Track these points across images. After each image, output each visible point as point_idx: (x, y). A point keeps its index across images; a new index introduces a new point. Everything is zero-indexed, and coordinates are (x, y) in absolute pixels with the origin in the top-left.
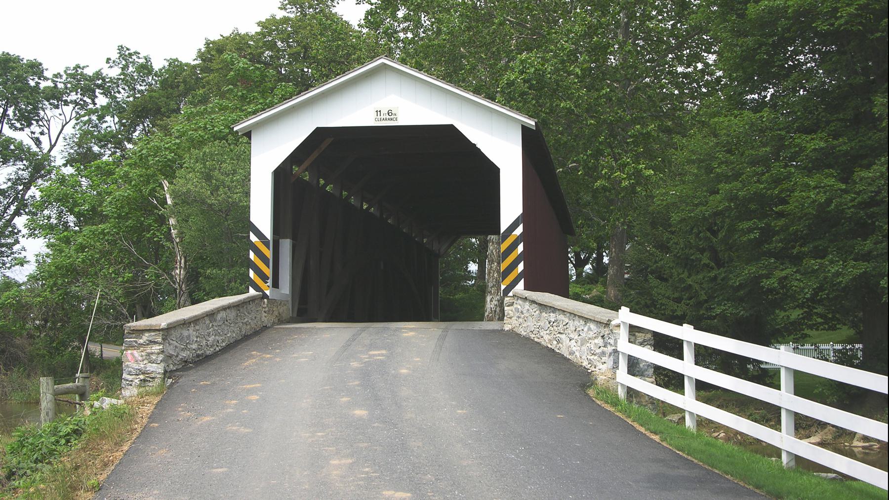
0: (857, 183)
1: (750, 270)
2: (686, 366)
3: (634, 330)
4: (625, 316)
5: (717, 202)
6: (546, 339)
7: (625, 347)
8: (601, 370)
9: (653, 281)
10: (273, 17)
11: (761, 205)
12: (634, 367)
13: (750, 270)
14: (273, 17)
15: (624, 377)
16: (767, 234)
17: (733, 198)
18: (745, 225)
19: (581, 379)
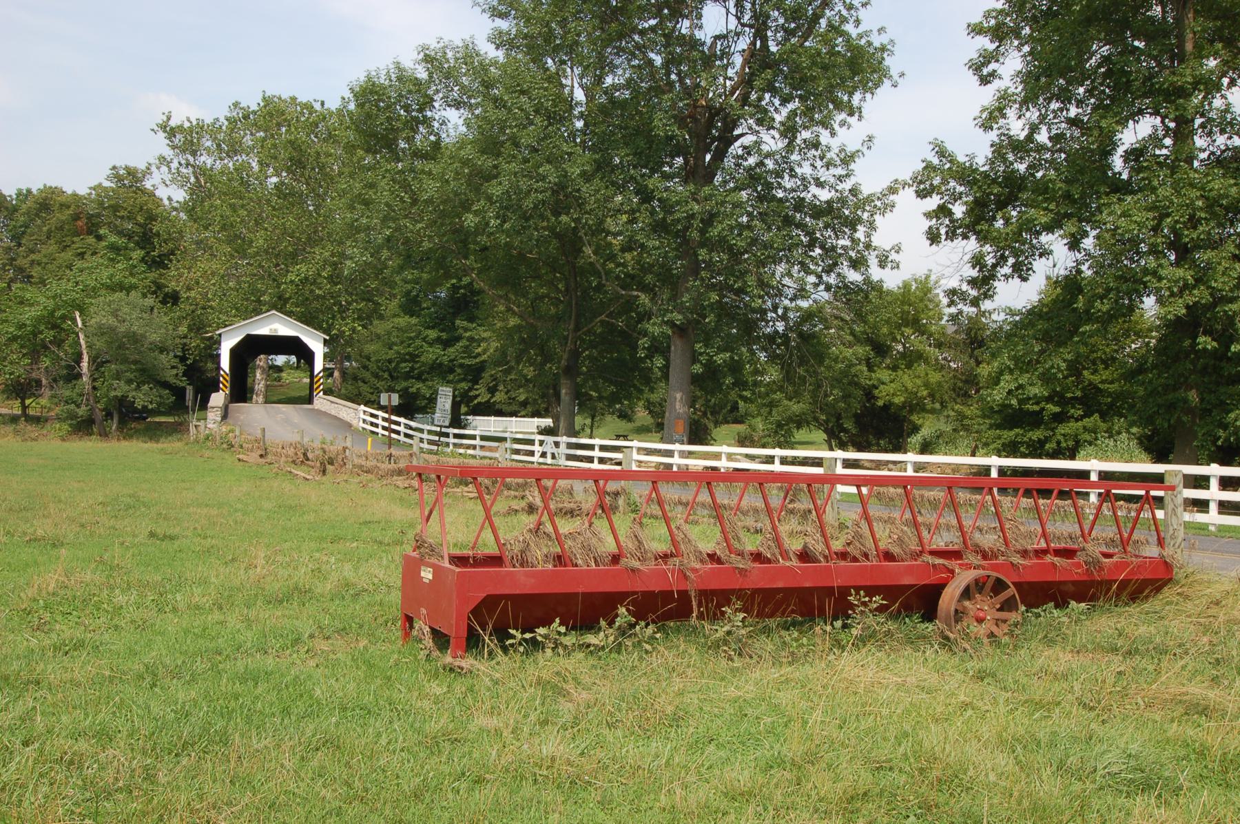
0: (690, 117)
1: (404, 384)
2: (380, 422)
3: (365, 412)
4: (362, 407)
5: (391, 354)
6: (333, 413)
7: (362, 416)
8: (354, 422)
9: (360, 384)
10: (100, 184)
11: (413, 357)
12: (364, 421)
13: (404, 384)
14: (100, 184)
15: (361, 424)
16: (412, 369)
17: (398, 353)
18: (403, 365)
19: (349, 425)
